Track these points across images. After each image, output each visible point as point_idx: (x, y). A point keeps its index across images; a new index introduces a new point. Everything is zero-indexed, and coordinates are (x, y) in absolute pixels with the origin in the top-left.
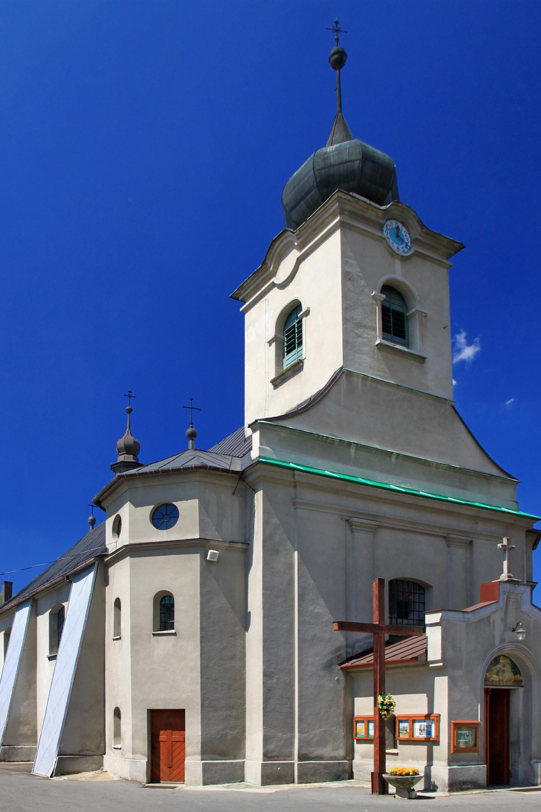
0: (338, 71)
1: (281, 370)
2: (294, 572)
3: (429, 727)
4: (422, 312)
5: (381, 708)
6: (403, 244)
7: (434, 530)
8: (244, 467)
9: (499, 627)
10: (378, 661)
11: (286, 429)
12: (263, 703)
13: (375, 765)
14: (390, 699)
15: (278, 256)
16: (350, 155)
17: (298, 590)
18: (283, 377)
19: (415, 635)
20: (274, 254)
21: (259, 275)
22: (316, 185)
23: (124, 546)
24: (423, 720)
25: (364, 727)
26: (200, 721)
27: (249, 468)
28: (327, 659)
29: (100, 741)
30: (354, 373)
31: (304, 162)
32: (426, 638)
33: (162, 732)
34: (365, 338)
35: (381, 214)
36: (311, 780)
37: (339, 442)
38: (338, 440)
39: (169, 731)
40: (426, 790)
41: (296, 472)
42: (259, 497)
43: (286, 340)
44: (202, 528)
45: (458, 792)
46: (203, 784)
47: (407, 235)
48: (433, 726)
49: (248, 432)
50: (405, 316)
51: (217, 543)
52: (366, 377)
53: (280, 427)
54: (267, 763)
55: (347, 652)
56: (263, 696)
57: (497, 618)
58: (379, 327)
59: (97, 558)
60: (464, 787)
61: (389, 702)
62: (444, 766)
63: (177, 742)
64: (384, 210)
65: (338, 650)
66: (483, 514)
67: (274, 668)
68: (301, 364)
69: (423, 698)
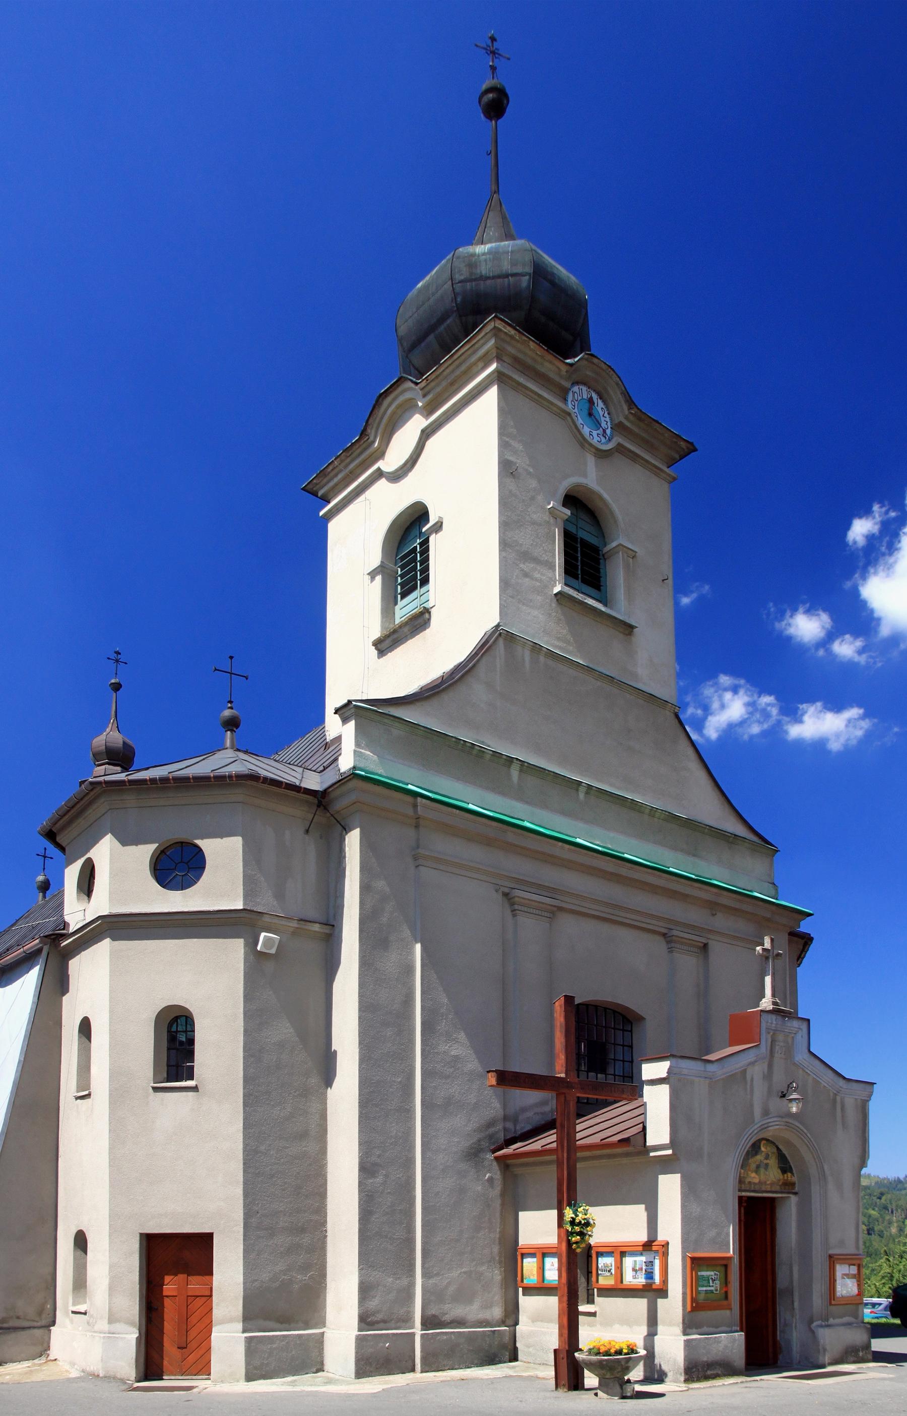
0: (493, 122)
1: (392, 626)
2: (414, 981)
3: (650, 1264)
4: (629, 548)
5: (570, 1230)
6: (599, 429)
8: (325, 786)
9: (759, 1090)
10: (565, 1144)
11: (401, 721)
12: (359, 1220)
13: (561, 1335)
14: (586, 1215)
15: (387, 425)
16: (514, 263)
17: (422, 1014)
18: (395, 636)
19: (625, 1099)
20: (382, 418)
21: (353, 456)
22: (455, 309)
23: (99, 916)
24: (639, 1253)
25: (535, 1265)
26: (242, 1255)
27: (335, 786)
28: (472, 1142)
29: (45, 1298)
30: (518, 638)
31: (436, 266)
32: (644, 1105)
33: (167, 1279)
34: (536, 580)
36: (444, 1365)
37: (492, 755)
39: (182, 1277)
40: (647, 1380)
41: (419, 799)
42: (353, 841)
43: (399, 573)
44: (250, 888)
45: (701, 1382)
48: (657, 1263)
49: (333, 726)
51: (276, 921)
52: (538, 646)
54: (366, 1335)
55: (505, 1129)
56: (359, 1207)
57: (757, 1072)
58: (559, 563)
59: (46, 939)
60: (709, 1372)
61: (584, 1219)
62: (675, 1335)
63: (197, 1296)
64: (571, 365)
65: (490, 1124)
66: (725, 900)
67: (379, 1156)
68: (427, 616)
69: (638, 1212)
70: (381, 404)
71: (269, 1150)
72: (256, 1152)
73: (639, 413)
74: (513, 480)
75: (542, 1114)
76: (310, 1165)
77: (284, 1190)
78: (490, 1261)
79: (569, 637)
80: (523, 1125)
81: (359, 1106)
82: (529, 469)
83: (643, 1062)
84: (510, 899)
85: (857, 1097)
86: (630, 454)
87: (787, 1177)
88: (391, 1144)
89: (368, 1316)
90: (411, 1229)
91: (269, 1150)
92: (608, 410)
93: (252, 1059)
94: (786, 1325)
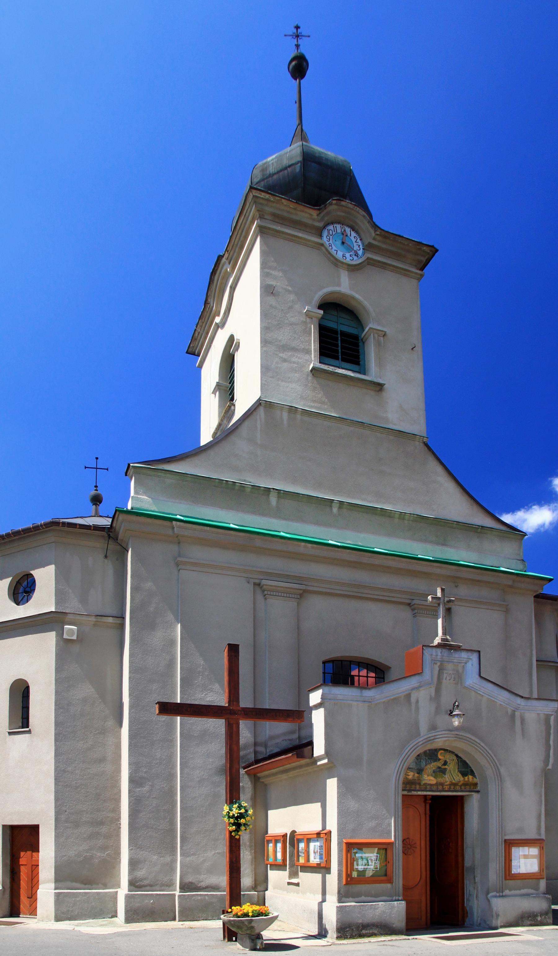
6: (352, 251)
7: (392, 595)
11: (171, 473)
26: (54, 839)
30: (275, 404)
33: (22, 854)
34: (294, 363)
35: (316, 215)
36: (199, 917)
39: (29, 853)
41: (174, 523)
46: (55, 920)
47: (357, 241)
50: (360, 338)
51: (78, 617)
52: (294, 408)
53: (163, 472)
55: (256, 752)
56: (129, 807)
60: (364, 932)
66: (464, 574)
67: (146, 772)
70: (213, 280)
71: (75, 770)
72: (64, 771)
73: (383, 233)
74: (274, 298)
75: (289, 740)
76: (107, 780)
77: (86, 797)
79: (324, 399)
80: (271, 749)
81: (129, 738)
82: (287, 288)
83: (310, 693)
84: (411, 606)
85: (538, 712)
86: (380, 264)
87: (468, 779)
88: (157, 764)
89: (137, 882)
90: (172, 822)
91: (75, 770)
92: (360, 237)
93: (61, 710)
94: (470, 895)
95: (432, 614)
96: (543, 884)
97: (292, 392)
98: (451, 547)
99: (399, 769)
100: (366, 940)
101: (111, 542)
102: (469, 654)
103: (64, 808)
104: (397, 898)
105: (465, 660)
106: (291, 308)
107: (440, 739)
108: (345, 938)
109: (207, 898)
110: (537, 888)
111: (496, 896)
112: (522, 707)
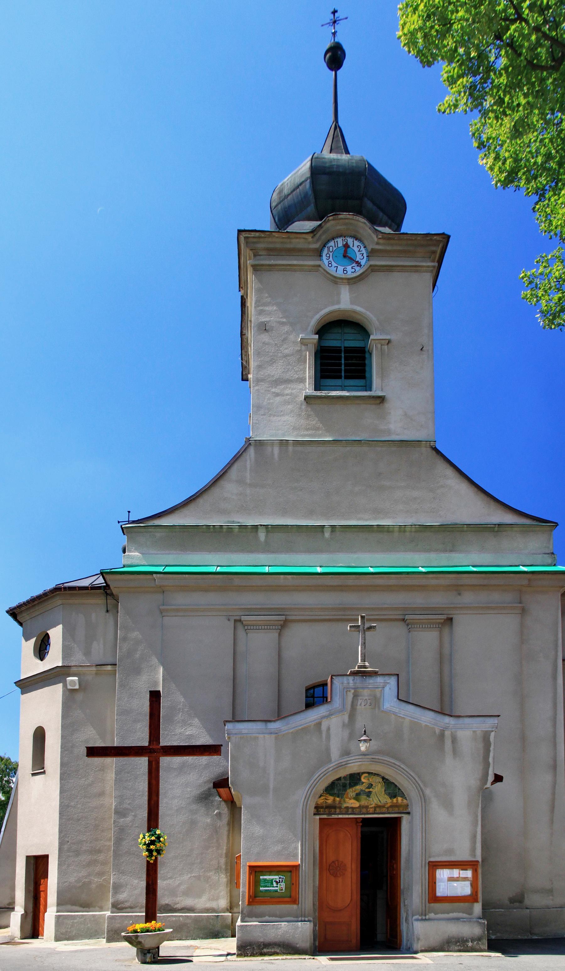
34: (287, 395)
35: (310, 237)
36: (174, 937)
38: (219, 527)
41: (154, 575)
52: (284, 441)
53: (153, 527)
60: (265, 950)
66: (466, 580)
67: (129, 804)
72: (68, 806)
73: (385, 236)
74: (267, 334)
77: (87, 828)
78: (217, 869)
87: (397, 800)
88: (139, 796)
89: (118, 904)
91: (77, 805)
93: (66, 752)
95: (426, 627)
96: (478, 908)
97: (285, 424)
98: (460, 552)
99: (307, 794)
100: (266, 958)
101: (109, 597)
102: (386, 678)
103: (67, 839)
104: (303, 919)
105: (381, 684)
106: (284, 340)
107: (352, 764)
108: (246, 955)
109: (181, 919)
110: (470, 912)
111: (417, 920)
112: (452, 725)
